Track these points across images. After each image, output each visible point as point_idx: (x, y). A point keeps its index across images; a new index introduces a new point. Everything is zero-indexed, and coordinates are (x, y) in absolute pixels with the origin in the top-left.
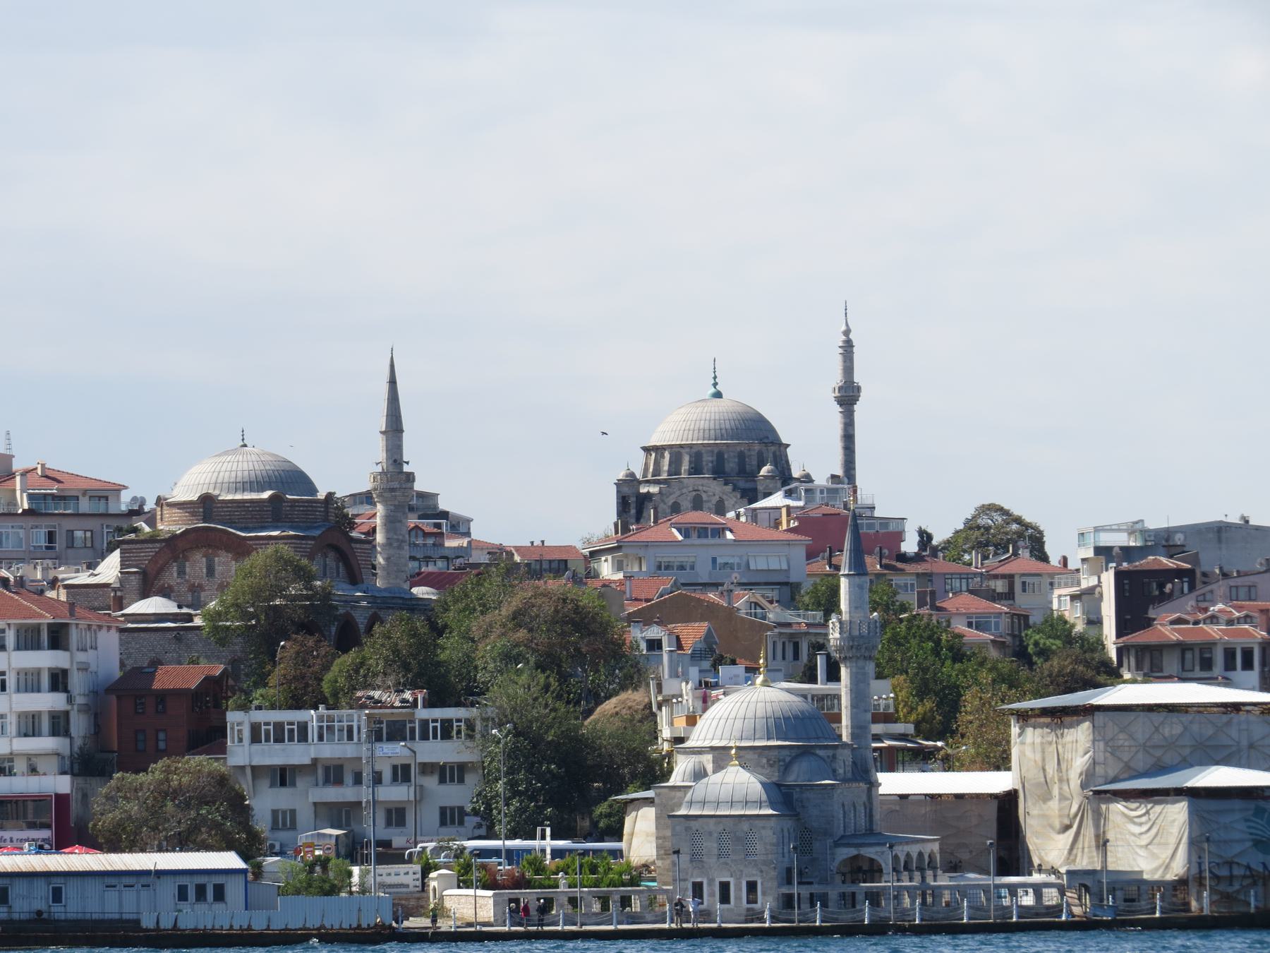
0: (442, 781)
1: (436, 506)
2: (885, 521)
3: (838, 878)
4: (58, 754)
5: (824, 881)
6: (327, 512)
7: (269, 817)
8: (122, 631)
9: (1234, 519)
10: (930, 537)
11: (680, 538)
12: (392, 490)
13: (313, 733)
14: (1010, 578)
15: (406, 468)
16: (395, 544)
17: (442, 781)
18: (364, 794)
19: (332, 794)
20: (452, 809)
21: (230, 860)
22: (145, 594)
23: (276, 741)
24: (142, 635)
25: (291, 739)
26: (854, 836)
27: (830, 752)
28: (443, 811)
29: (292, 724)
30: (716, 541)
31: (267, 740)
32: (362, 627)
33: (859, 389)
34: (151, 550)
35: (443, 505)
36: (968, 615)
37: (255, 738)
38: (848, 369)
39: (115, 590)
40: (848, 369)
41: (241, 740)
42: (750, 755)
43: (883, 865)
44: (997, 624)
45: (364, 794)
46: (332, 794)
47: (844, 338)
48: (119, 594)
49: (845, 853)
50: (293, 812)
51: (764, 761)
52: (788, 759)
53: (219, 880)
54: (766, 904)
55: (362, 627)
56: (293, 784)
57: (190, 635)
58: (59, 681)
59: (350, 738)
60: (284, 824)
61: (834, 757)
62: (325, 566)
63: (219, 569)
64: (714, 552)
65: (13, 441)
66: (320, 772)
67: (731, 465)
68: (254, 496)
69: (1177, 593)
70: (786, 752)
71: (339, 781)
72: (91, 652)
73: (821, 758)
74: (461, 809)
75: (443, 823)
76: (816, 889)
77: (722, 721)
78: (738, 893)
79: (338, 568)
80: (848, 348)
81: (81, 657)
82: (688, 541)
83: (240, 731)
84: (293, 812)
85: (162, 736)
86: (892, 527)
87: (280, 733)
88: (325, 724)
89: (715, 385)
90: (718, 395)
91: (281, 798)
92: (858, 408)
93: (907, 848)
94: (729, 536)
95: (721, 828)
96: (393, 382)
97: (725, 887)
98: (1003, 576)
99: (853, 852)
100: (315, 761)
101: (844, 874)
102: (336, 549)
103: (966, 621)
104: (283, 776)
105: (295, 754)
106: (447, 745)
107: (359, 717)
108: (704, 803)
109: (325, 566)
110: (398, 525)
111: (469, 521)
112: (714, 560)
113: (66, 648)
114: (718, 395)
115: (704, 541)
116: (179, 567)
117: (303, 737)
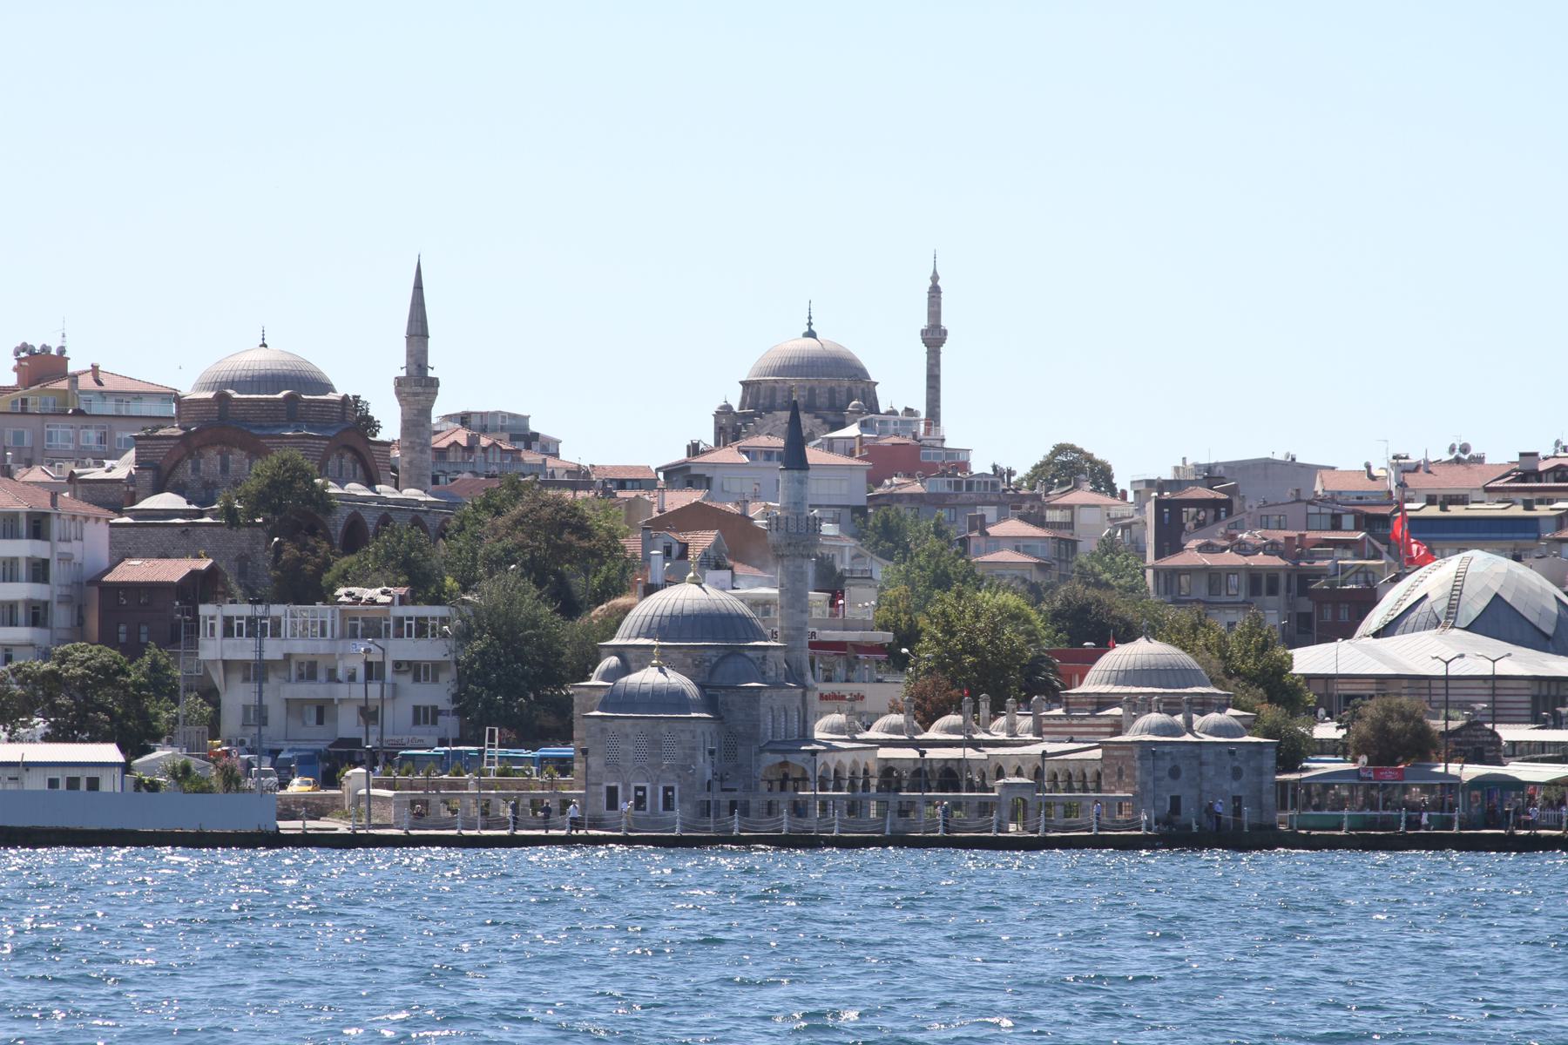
0: (417, 679)
1: (527, 428)
2: (953, 453)
3: (764, 786)
4: (32, 645)
5: (748, 788)
6: (344, 413)
8: (112, 525)
9: (1280, 456)
15: (431, 374)
17: (417, 679)
18: (342, 691)
19: (304, 690)
20: (426, 709)
21: (109, 753)
22: (158, 489)
23: (248, 635)
26: (783, 742)
27: (760, 654)
28: (416, 709)
32: (371, 528)
33: (945, 332)
35: (534, 427)
37: (228, 631)
41: (212, 635)
42: (675, 655)
46: (304, 690)
49: (771, 759)
52: (714, 660)
53: (93, 773)
55: (371, 528)
57: (199, 530)
58: (39, 570)
59: (323, 634)
61: (764, 658)
62: (341, 466)
63: (232, 466)
66: (293, 667)
67: (822, 400)
69: (1209, 520)
72: (75, 543)
73: (750, 660)
74: (434, 708)
75: (416, 721)
76: (737, 796)
80: (935, 292)
81: (64, 547)
82: (755, 464)
83: (212, 626)
85: (144, 629)
86: (962, 458)
89: (810, 324)
92: (945, 350)
93: (838, 756)
96: (418, 287)
99: (779, 758)
100: (288, 657)
101: (770, 782)
104: (258, 671)
106: (422, 642)
109: (341, 466)
111: (558, 442)
113: (46, 538)
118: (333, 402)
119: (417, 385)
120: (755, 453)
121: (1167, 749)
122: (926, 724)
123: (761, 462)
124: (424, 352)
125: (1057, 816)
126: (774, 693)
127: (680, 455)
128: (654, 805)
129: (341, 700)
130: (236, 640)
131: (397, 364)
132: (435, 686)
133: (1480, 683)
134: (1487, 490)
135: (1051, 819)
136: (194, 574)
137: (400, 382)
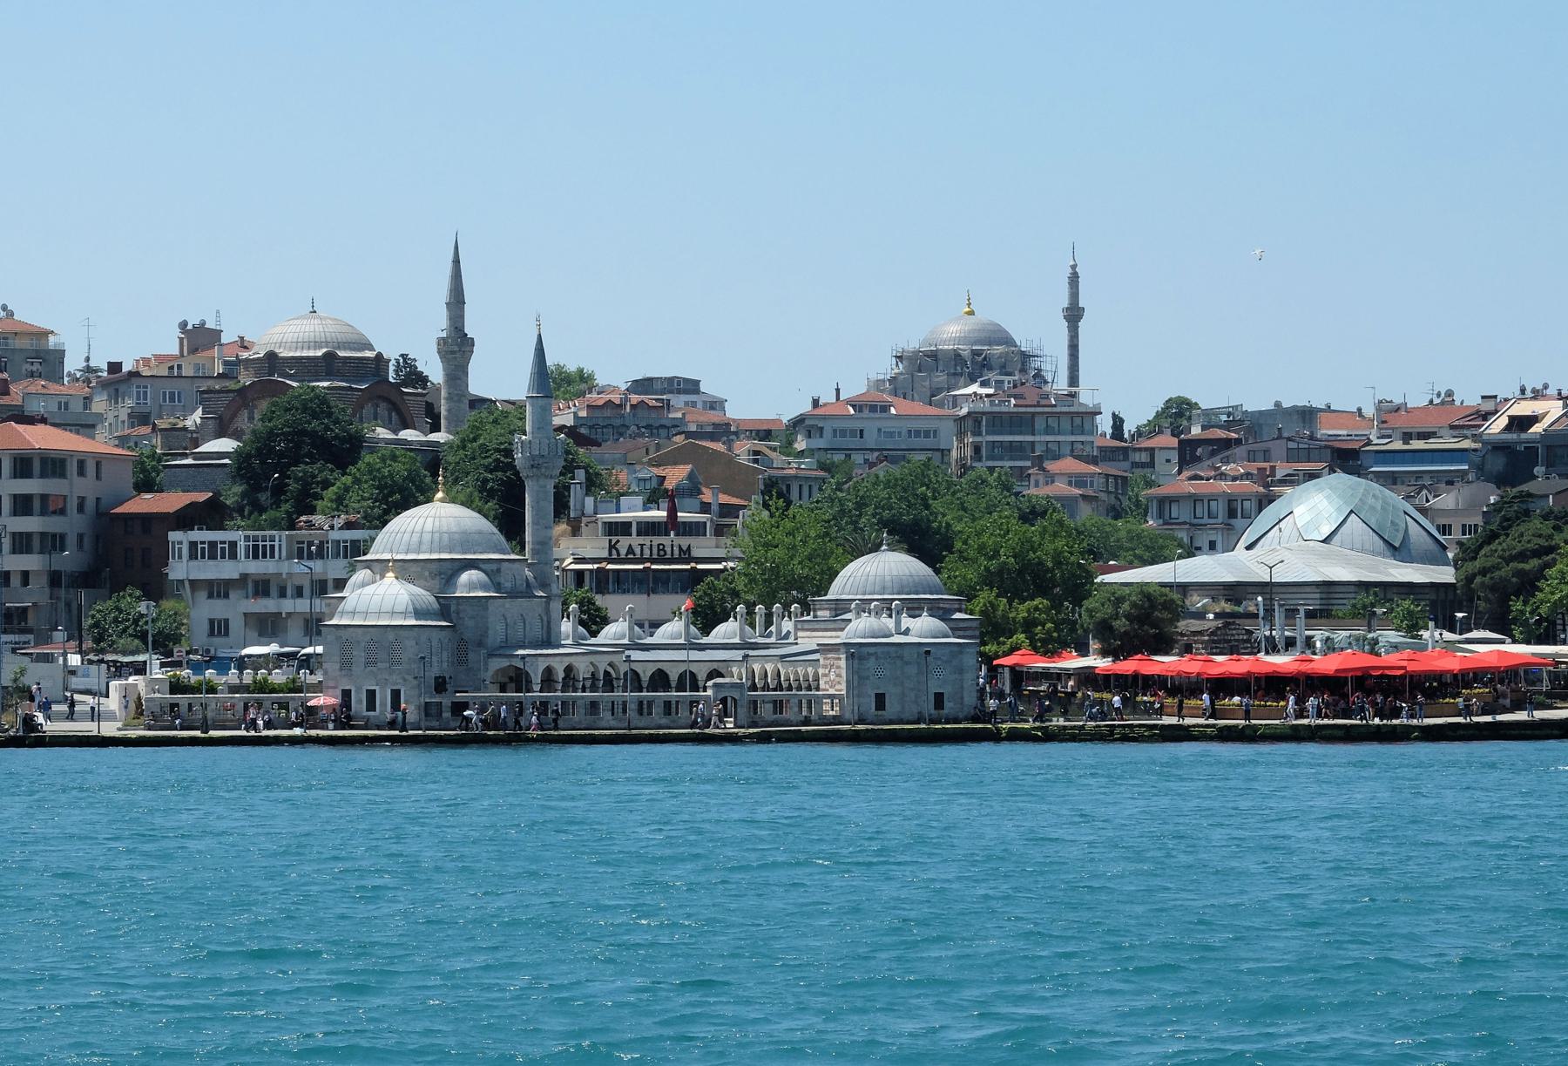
7: (206, 626)
10: (1122, 421)
12: (453, 352)
13: (241, 551)
14: (1151, 451)
25: (223, 557)
28: (212, 622)
31: (223, 557)
34: (226, 399)
36: (1070, 475)
39: (192, 432)
41: (180, 557)
42: (414, 568)
45: (288, 605)
49: (497, 664)
50: (227, 621)
56: (227, 596)
61: (499, 570)
64: (878, 424)
66: (250, 585)
68: (311, 353)
70: (448, 565)
75: (212, 634)
80: (1074, 279)
84: (227, 621)
87: (213, 551)
90: (971, 313)
94: (893, 411)
95: (368, 638)
96: (456, 262)
97: (371, 695)
98: (1146, 449)
103: (1066, 479)
104: (218, 589)
105: (226, 570)
108: (354, 613)
114: (971, 313)
117: (233, 556)
118: (368, 359)
119: (457, 347)
121: (872, 650)
122: (706, 630)
124: (462, 317)
125: (766, 711)
126: (508, 603)
127: (807, 407)
128: (383, 704)
129: (289, 614)
130: (198, 563)
131: (439, 323)
133: (1314, 589)
134: (1452, 427)
137: (442, 342)
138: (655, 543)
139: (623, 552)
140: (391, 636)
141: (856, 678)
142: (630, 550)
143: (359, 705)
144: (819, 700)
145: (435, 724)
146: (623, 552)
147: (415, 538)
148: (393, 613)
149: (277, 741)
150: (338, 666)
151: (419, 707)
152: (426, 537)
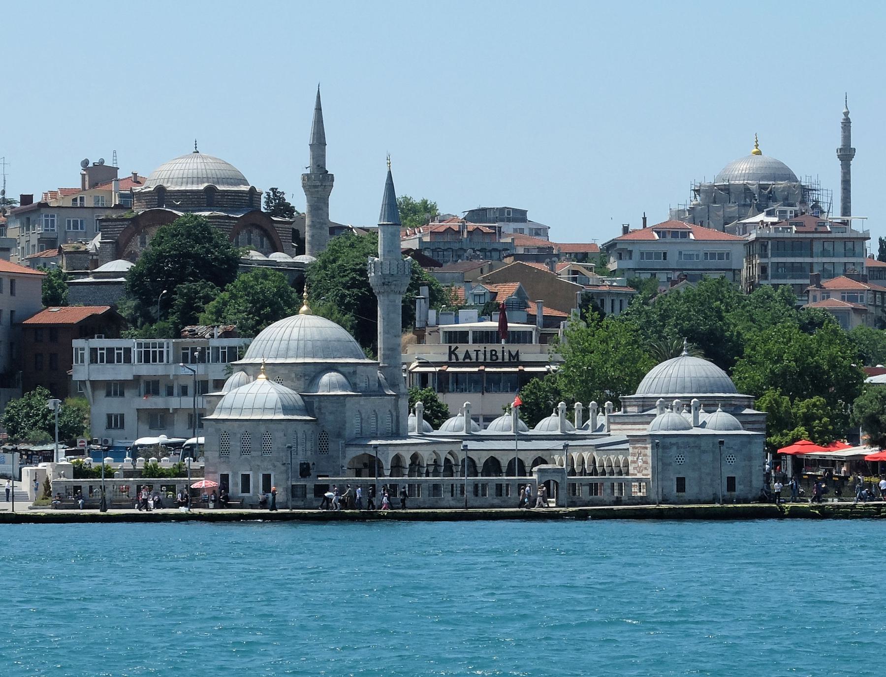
7: (104, 420)
11: (657, 238)
12: (315, 187)
13: (134, 356)
16: (318, 226)
18: (174, 402)
24: (104, 286)
25: (119, 361)
28: (109, 416)
29: (121, 349)
30: (684, 240)
31: (102, 361)
34: (121, 227)
36: (843, 292)
37: (93, 360)
38: (847, 137)
39: (92, 255)
40: (847, 137)
41: (82, 361)
42: (283, 371)
43: (384, 462)
44: (862, 298)
45: (174, 402)
46: (157, 402)
47: (843, 117)
48: (95, 257)
49: (353, 452)
50: (122, 416)
51: (293, 375)
54: (280, 493)
60: (116, 425)
61: (355, 372)
65: (118, 158)
66: (142, 385)
68: (195, 187)
71: (156, 392)
75: (109, 426)
77: (265, 342)
78: (256, 481)
79: (262, 242)
80: (847, 124)
82: (663, 240)
83: (82, 354)
87: (110, 356)
88: (143, 349)
89: (757, 146)
90: (759, 153)
91: (114, 405)
94: (692, 236)
95: (243, 430)
96: (319, 109)
97: (246, 478)
102: (258, 227)
103: (840, 295)
104: (116, 389)
107: (168, 344)
110: (320, 212)
112: (680, 253)
114: (759, 153)
115: (674, 240)
116: (141, 239)
117: (128, 360)
120: (664, 233)
121: (674, 440)
123: (669, 238)
124: (323, 156)
126: (362, 401)
127: (618, 234)
128: (256, 487)
129: (176, 410)
130: (98, 366)
131: (304, 162)
132: (121, 399)
135: (592, 500)
136: (93, 317)
137: (306, 178)
138: (488, 349)
139: (461, 357)
140: (263, 428)
141: (660, 465)
142: (467, 355)
143: (235, 487)
144: (629, 483)
145: (301, 503)
146: (461, 357)
147: (284, 345)
148: (253, 409)
149: (165, 518)
150: (217, 454)
151: (286, 489)
152: (293, 344)
